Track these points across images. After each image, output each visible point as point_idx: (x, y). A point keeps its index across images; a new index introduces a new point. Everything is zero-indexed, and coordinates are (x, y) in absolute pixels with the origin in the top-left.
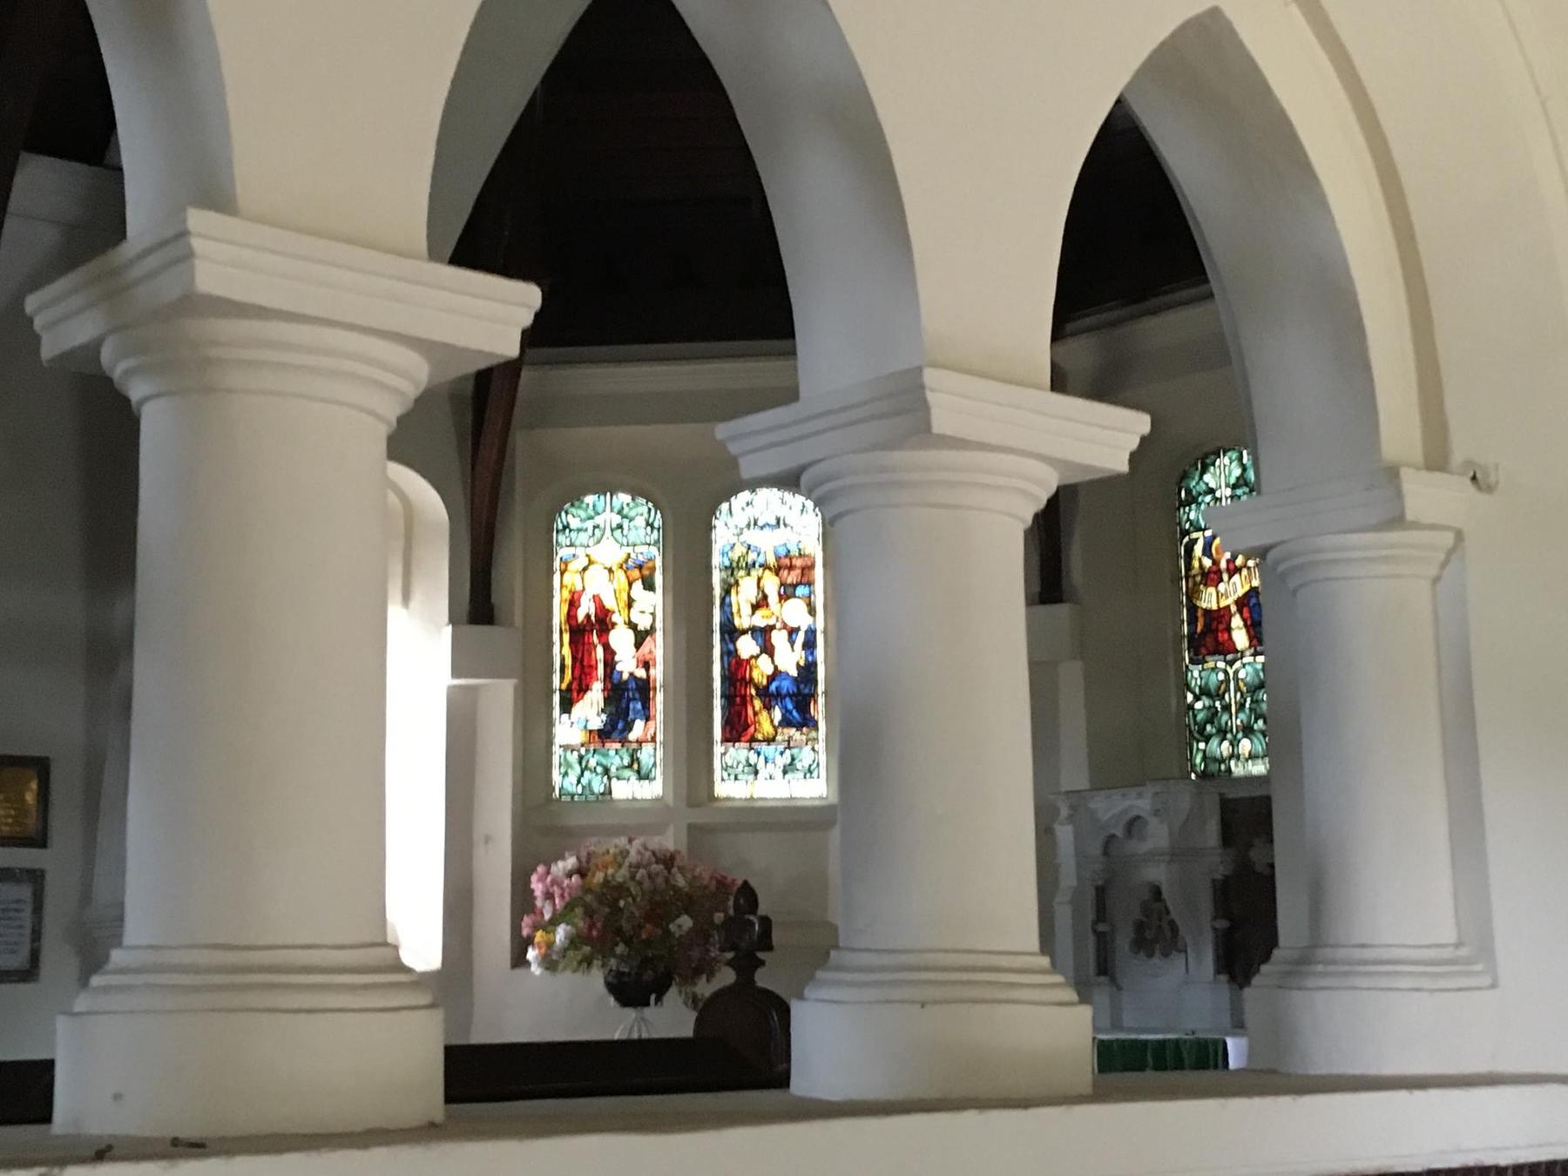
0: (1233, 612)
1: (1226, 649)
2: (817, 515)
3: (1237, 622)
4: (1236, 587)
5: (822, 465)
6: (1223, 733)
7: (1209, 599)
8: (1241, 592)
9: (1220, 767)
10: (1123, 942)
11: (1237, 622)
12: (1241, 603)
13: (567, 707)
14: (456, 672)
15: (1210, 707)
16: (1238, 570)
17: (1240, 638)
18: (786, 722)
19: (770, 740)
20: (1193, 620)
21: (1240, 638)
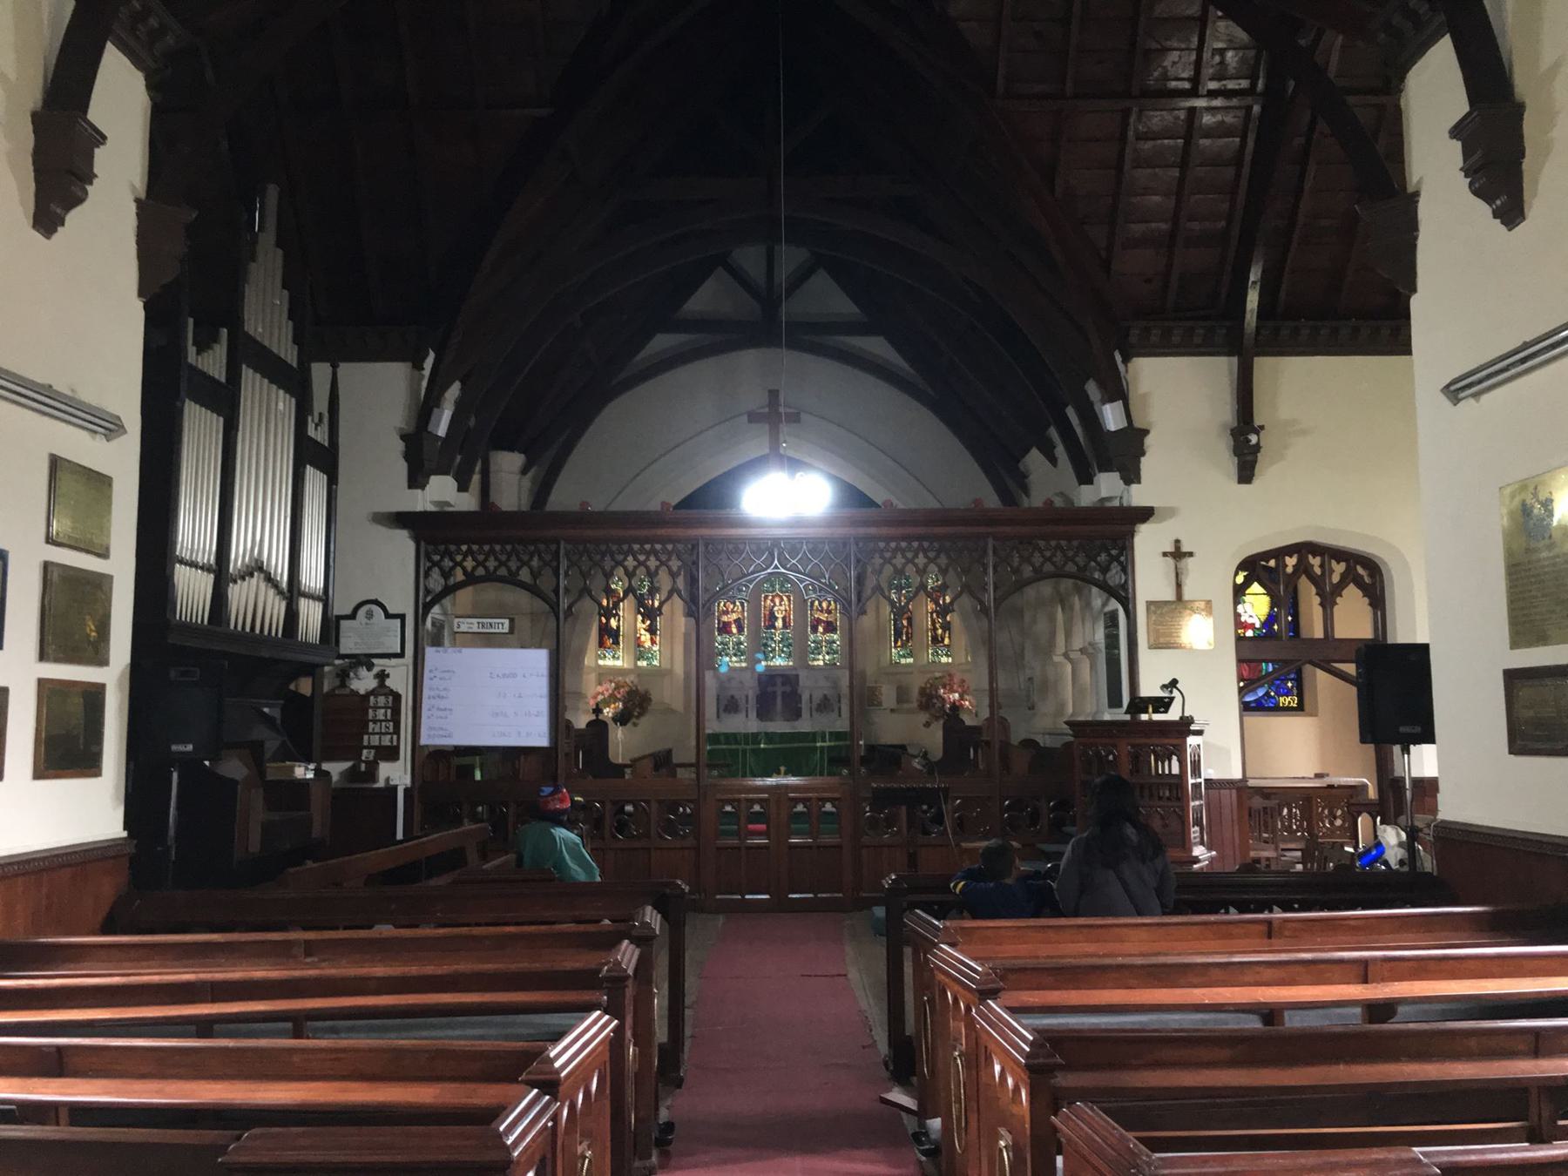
0: (466, 502)
1: (729, 632)
2: (1178, 554)
3: (733, 626)
4: (735, 616)
5: (240, 608)
6: (727, 655)
7: (725, 619)
8: (735, 618)
9: (585, 583)
10: (721, 711)
11: (733, 626)
12: (735, 621)
13: (580, 1143)
14: (779, 345)
15: (927, 764)
16: (734, 612)
17: (734, 630)
18: (613, 643)
19: (609, 648)
20: (719, 624)
21: (734, 630)
